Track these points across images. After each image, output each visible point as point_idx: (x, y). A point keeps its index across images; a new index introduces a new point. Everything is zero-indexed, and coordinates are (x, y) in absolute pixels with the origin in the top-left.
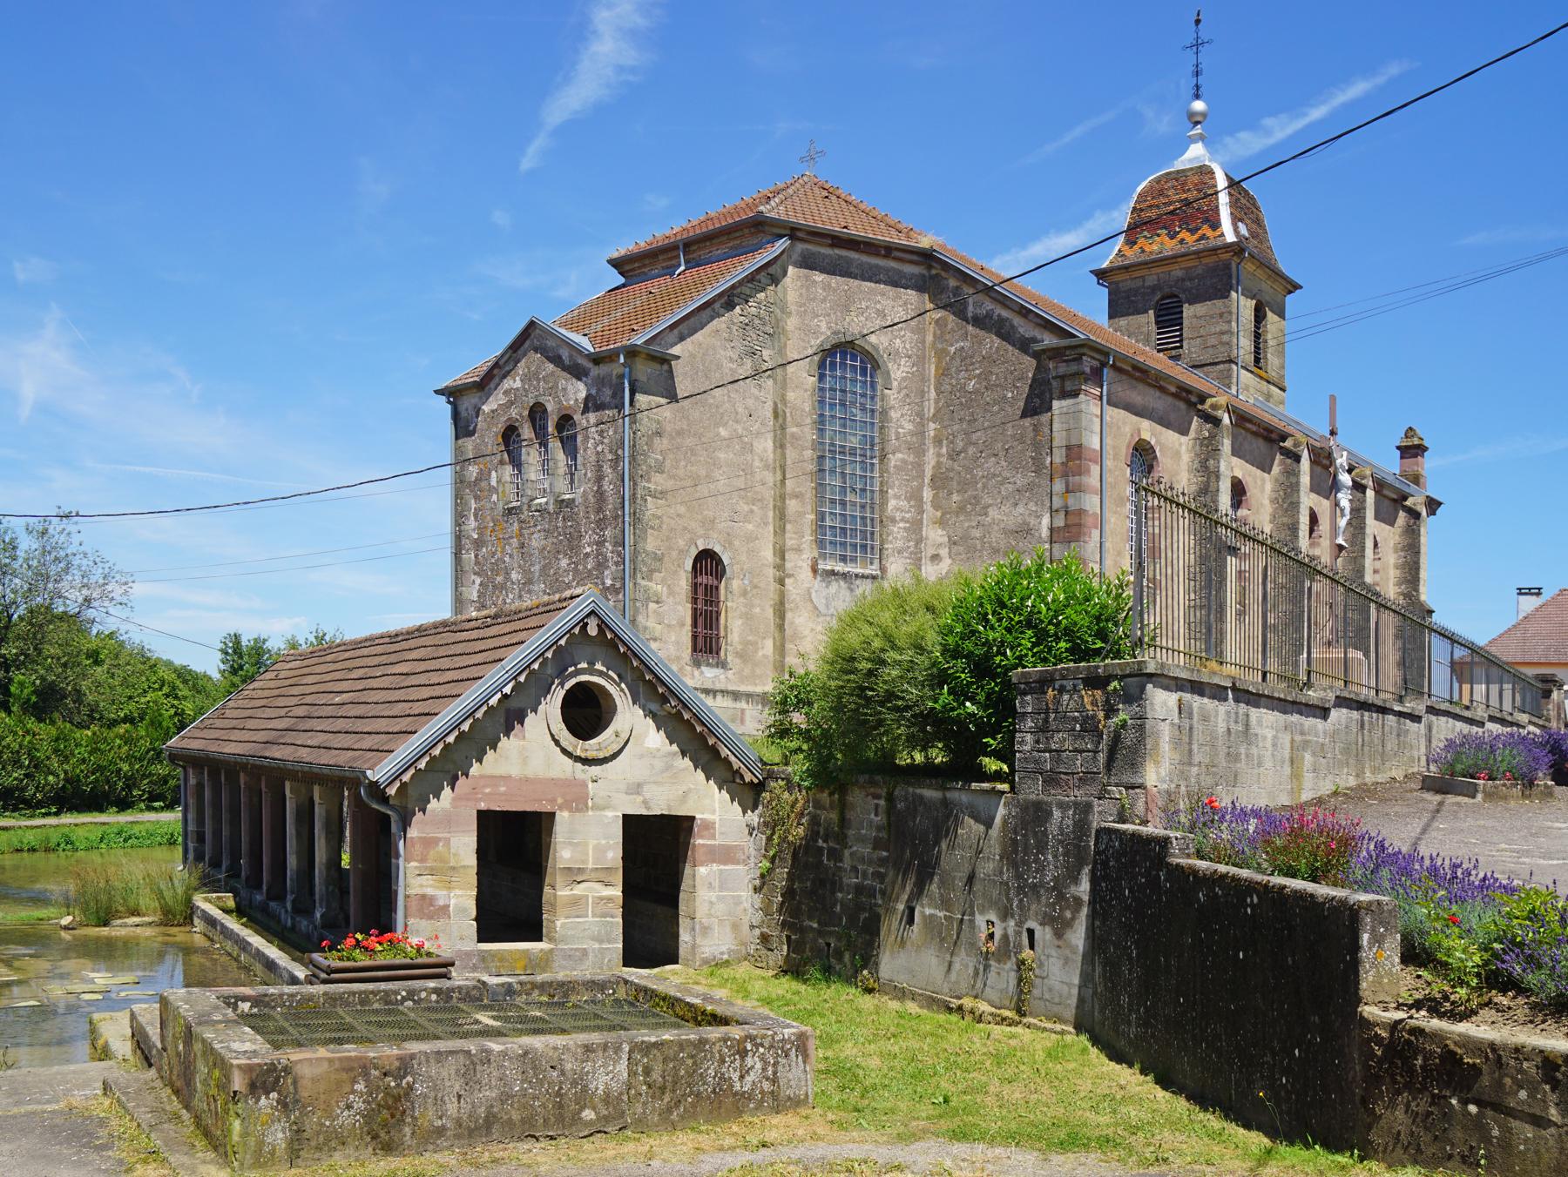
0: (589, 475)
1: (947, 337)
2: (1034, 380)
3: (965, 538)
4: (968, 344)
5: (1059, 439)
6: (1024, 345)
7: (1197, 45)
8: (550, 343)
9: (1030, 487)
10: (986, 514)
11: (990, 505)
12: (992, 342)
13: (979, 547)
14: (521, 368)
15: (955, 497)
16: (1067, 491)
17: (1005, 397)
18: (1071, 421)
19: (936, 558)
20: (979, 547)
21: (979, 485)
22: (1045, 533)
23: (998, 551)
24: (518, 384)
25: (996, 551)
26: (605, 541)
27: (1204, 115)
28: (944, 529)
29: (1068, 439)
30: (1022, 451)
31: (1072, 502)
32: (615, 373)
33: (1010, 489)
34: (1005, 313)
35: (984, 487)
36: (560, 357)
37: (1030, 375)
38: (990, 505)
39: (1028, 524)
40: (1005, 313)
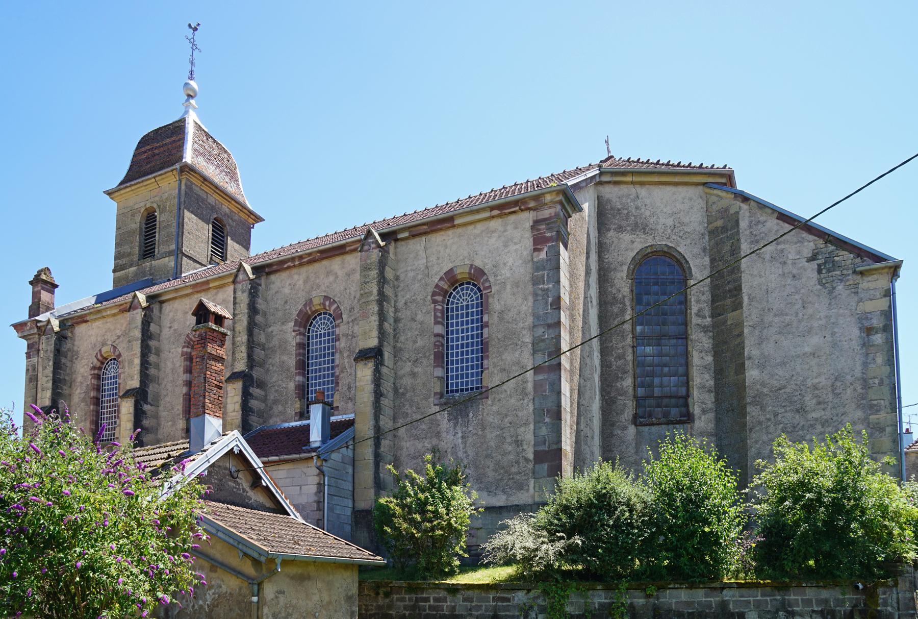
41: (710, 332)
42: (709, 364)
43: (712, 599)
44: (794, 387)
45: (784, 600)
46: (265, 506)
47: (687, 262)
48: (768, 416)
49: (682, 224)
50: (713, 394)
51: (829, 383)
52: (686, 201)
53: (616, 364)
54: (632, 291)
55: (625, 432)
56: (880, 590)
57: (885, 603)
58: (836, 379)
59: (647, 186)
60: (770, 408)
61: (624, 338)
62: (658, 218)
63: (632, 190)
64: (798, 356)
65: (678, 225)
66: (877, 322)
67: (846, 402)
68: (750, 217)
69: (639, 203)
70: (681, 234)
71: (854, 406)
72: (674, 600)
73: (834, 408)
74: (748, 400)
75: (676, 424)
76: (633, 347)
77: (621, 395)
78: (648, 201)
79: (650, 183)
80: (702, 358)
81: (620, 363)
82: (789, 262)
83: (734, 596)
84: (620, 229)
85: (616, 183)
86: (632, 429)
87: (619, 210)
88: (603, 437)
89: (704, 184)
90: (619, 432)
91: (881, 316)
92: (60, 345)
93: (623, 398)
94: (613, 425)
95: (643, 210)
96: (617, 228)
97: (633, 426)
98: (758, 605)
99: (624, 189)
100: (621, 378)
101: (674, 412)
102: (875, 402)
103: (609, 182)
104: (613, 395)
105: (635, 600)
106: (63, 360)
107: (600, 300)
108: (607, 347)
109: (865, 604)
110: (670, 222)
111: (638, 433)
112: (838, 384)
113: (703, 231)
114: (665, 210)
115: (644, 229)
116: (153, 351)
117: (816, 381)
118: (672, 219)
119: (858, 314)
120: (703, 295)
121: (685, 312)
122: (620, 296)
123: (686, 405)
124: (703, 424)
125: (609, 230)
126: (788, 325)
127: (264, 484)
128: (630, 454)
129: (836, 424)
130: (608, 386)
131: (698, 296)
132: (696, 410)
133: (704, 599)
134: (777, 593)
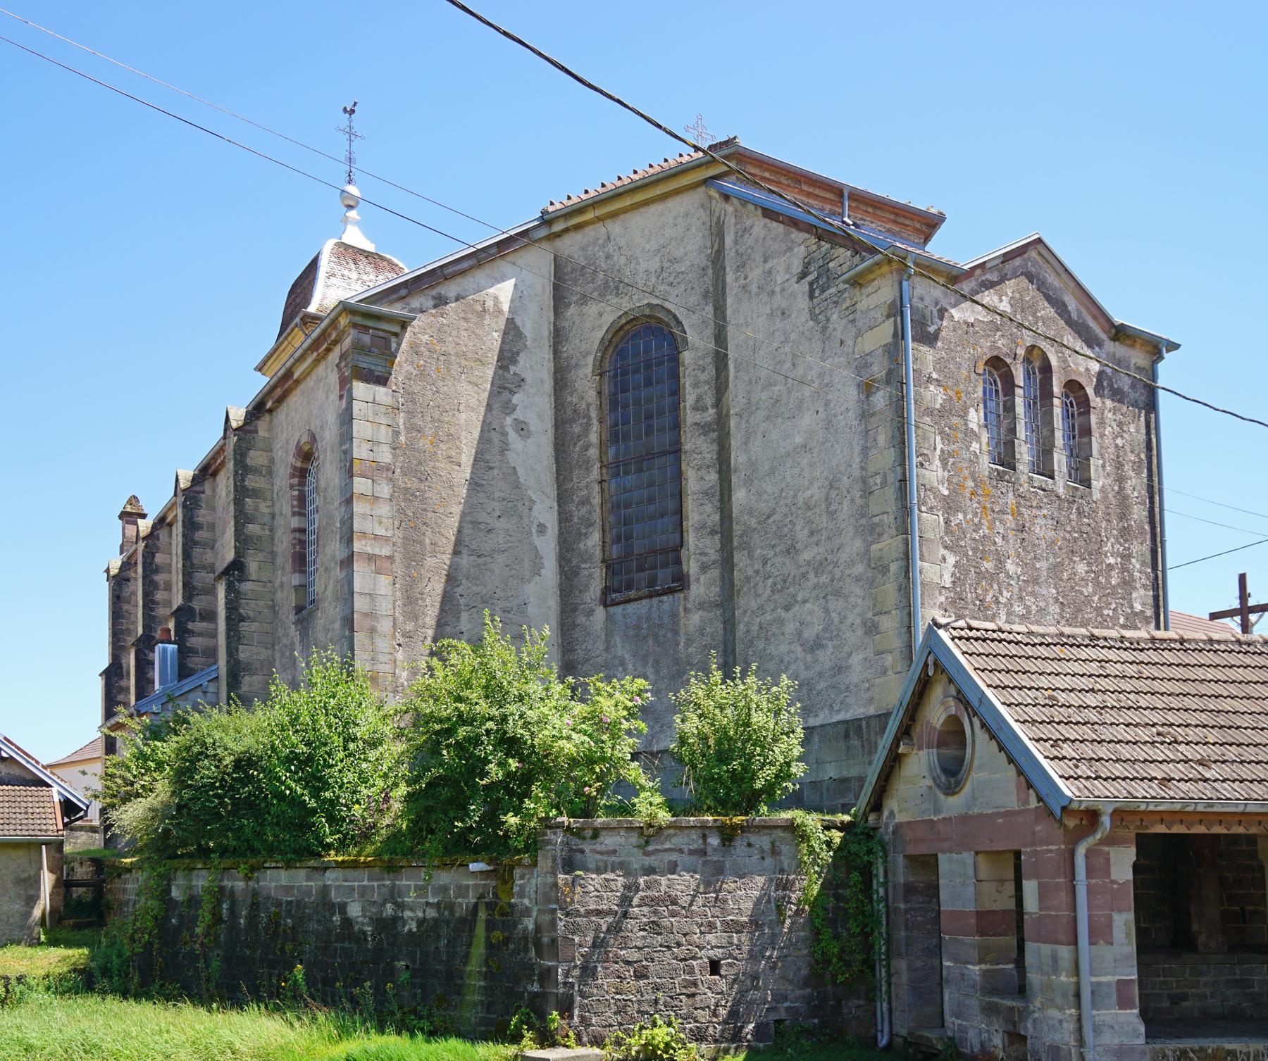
36: (1064, 305)
41: (714, 431)
42: (712, 487)
43: (313, 884)
44: (784, 510)
45: (394, 886)
46: (24, 779)
47: (679, 323)
48: (756, 567)
49: (673, 261)
50: (717, 537)
51: (823, 496)
52: (680, 220)
53: (578, 513)
54: (600, 393)
55: (591, 618)
56: (517, 872)
57: (522, 895)
58: (831, 486)
59: (622, 217)
60: (759, 551)
61: (588, 470)
62: (638, 263)
63: (599, 231)
64: (788, 455)
65: (666, 265)
66: (878, 369)
67: (843, 526)
68: (736, 224)
69: (610, 248)
70: (671, 279)
71: (851, 530)
72: (274, 884)
73: (829, 538)
74: (735, 544)
75: (663, 594)
76: (601, 482)
77: (585, 562)
78: (622, 242)
79: (625, 210)
80: (702, 478)
81: (584, 510)
82: (778, 289)
83: (337, 879)
84: (584, 300)
85: (578, 227)
86: (600, 613)
87: (583, 268)
88: (562, 630)
89: (705, 182)
90: (584, 619)
91: (884, 355)
92: (121, 590)
93: (587, 566)
94: (575, 610)
95: (615, 259)
96: (581, 299)
97: (601, 607)
98: (363, 891)
99: (590, 232)
100: (586, 534)
101: (664, 575)
102: (876, 520)
103: (566, 230)
104: (574, 562)
105: (236, 883)
106: (125, 607)
107: (556, 419)
108: (566, 490)
109: (496, 895)
110: (655, 265)
111: (609, 618)
112: (833, 494)
113: (705, 262)
114: (648, 247)
115: (617, 288)
116: (162, 586)
117: (808, 494)
118: (657, 259)
119: (856, 360)
120: (703, 372)
121: (676, 408)
122: (584, 406)
123: (678, 561)
124: (702, 590)
125: (568, 305)
126: (777, 401)
127: (4, 755)
128: (598, 652)
129: (830, 568)
130: (568, 550)
131: (696, 376)
132: (692, 567)
133: (305, 884)
134: (386, 876)
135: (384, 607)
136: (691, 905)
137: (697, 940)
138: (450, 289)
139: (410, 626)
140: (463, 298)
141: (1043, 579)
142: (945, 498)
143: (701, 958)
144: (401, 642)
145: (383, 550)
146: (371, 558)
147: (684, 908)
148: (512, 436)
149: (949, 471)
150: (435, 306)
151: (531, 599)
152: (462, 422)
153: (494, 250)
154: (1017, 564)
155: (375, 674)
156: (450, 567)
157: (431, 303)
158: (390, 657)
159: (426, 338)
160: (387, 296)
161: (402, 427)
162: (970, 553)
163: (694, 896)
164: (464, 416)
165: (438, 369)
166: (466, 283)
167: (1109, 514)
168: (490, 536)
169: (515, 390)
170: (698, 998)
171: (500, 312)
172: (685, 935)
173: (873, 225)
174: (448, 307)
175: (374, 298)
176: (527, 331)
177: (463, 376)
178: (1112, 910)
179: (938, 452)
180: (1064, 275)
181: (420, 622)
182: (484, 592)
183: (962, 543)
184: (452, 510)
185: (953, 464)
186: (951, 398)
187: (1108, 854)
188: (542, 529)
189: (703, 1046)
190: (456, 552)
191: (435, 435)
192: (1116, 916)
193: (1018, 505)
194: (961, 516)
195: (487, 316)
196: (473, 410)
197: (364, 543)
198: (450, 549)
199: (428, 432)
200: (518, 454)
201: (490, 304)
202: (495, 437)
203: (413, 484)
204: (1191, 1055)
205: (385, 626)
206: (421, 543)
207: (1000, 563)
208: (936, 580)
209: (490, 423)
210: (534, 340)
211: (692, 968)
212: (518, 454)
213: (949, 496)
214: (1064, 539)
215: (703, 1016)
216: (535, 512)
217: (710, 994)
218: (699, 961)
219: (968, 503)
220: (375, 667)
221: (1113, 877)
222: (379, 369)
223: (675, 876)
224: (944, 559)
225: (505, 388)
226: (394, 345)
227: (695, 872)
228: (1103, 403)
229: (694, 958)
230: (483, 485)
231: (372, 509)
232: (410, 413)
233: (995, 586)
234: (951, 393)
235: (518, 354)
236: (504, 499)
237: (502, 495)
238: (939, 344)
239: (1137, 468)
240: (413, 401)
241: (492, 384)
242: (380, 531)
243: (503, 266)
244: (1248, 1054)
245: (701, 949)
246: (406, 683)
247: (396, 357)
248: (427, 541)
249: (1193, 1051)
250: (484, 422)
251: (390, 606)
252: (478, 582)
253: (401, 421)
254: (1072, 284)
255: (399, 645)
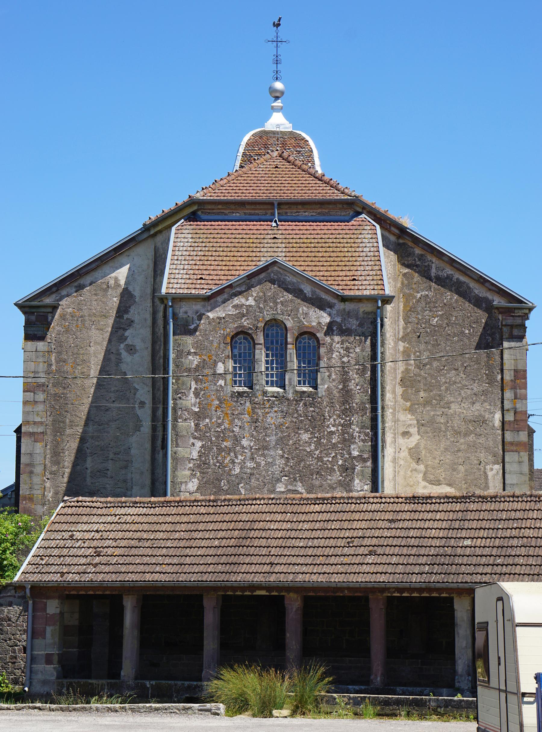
0: (334, 377)
1: (414, 286)
2: (486, 323)
3: (432, 421)
4: (431, 294)
5: (508, 364)
6: (478, 302)
7: (277, 41)
8: (290, 278)
9: (485, 393)
10: (449, 408)
11: (453, 402)
12: (450, 297)
13: (443, 429)
14: (255, 292)
15: (422, 394)
16: (516, 398)
17: (463, 333)
18: (518, 355)
19: (406, 434)
20: (443, 429)
21: (443, 388)
22: (497, 423)
23: (460, 433)
24: (251, 301)
25: (457, 433)
26: (351, 424)
27: (282, 93)
28: (413, 414)
29: (516, 365)
30: (479, 369)
31: (519, 406)
32: (362, 310)
33: (469, 392)
34: (463, 278)
35: (447, 389)
36: (301, 291)
37: (483, 321)
38: (453, 402)
39: (484, 417)
40: (463, 278)
135: (38, 459)
136: (17, 621)
137: (18, 638)
138: (87, 279)
139: (54, 468)
140: (94, 283)
141: (272, 446)
142: (196, 413)
143: (19, 646)
144: (49, 477)
145: (39, 429)
146: (32, 434)
147: (14, 623)
148: (124, 354)
149: (200, 398)
150: (76, 292)
151: (134, 445)
152: (92, 352)
153: (113, 253)
154: (251, 441)
155: (32, 496)
156: (82, 433)
157: (74, 290)
158: (41, 486)
159: (70, 310)
160: (45, 293)
161: (53, 361)
162: (214, 439)
163: (19, 617)
164: (93, 348)
165: (77, 326)
166: (97, 274)
167: (332, 403)
168: (108, 413)
169: (127, 328)
170: (16, 664)
171: (119, 285)
172: (13, 635)
173: (307, 214)
174: (84, 290)
175: (36, 296)
176: (137, 293)
177: (93, 327)
178: (46, 625)
179: (193, 389)
180: (297, 275)
181: (61, 465)
182: (103, 444)
183: (208, 434)
184: (84, 402)
185: (204, 394)
186: (204, 360)
187: (46, 603)
188: (142, 404)
189: (17, 686)
190: (86, 424)
191: (75, 362)
192: (48, 628)
193: (253, 409)
194: (207, 420)
195: (110, 290)
196: (99, 344)
197: (28, 427)
198: (83, 423)
199: (70, 361)
200: (127, 364)
201: (112, 282)
202: (113, 357)
203: (60, 391)
204: (74, 684)
205: (39, 469)
206: (64, 422)
207: (237, 440)
208: (186, 456)
209: (110, 350)
210: (141, 297)
211: (15, 650)
212: (127, 364)
213: (199, 412)
214: (292, 422)
215: (18, 672)
216: (138, 395)
217: (22, 663)
218: (18, 647)
219: (214, 413)
220: (32, 492)
221: (47, 612)
222: (40, 333)
223: (11, 608)
224: (193, 444)
225: (121, 328)
226: (50, 318)
227: (20, 606)
228: (332, 339)
229: (16, 646)
230: (104, 385)
231: (33, 408)
232: (59, 353)
233: (232, 454)
234: (205, 358)
235: (130, 307)
236: (117, 391)
237: (116, 388)
238: (197, 333)
239: (362, 373)
240: (61, 346)
241: (112, 328)
242: (38, 419)
243: (123, 259)
244: (98, 685)
245: (20, 642)
246: (51, 499)
247: (51, 324)
248: (68, 420)
249: (75, 682)
250: (106, 350)
251: (42, 459)
252: (99, 440)
253: (53, 359)
254: (305, 279)
255: (48, 479)
